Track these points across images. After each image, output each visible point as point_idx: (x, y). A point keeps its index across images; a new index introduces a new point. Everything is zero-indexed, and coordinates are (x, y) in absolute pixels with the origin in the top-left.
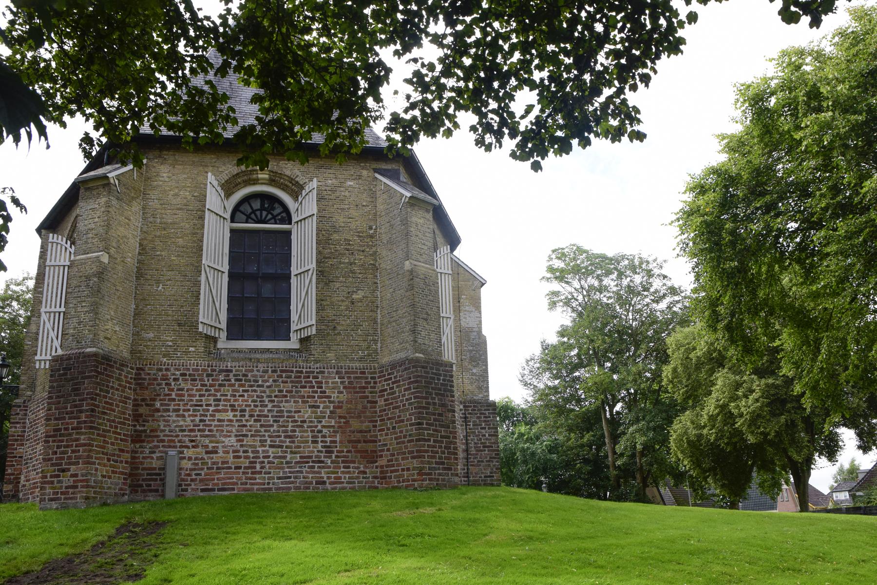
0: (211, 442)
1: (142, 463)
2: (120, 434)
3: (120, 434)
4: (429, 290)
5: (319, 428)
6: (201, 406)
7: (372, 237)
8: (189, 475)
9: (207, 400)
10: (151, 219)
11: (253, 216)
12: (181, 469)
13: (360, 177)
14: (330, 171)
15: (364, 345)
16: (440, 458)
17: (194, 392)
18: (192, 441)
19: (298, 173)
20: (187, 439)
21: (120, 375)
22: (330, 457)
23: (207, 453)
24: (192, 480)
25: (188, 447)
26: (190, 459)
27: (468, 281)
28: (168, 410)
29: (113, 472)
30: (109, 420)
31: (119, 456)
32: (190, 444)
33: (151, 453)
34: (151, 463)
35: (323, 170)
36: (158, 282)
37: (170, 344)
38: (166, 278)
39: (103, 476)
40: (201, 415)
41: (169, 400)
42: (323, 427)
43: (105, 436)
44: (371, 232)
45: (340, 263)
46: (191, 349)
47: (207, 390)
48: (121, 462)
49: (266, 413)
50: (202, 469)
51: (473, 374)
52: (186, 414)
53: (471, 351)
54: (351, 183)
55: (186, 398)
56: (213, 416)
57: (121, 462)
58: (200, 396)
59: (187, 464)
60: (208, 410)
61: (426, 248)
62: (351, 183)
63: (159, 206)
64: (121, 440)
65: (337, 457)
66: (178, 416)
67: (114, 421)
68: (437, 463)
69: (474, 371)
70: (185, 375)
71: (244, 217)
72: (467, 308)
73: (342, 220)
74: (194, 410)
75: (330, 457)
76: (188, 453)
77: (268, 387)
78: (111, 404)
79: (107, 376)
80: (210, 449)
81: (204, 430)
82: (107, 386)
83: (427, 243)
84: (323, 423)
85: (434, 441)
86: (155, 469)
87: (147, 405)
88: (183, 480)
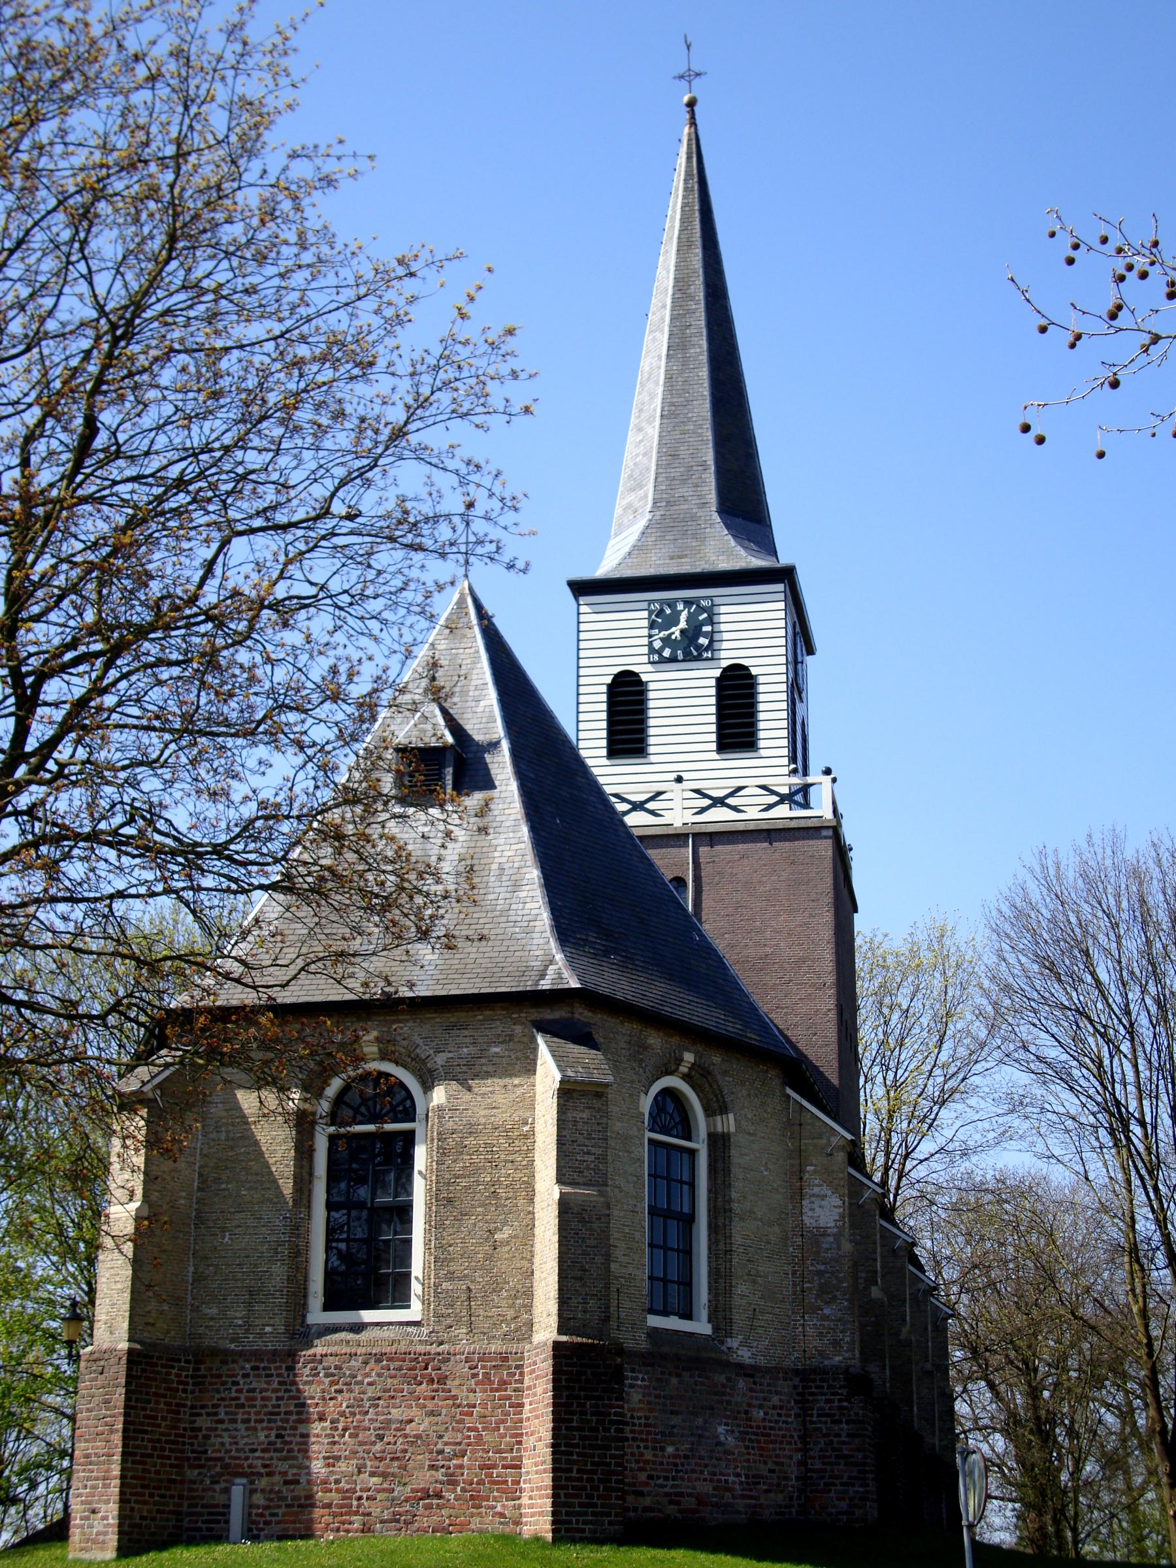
0: (291, 1467)
1: (202, 1498)
2: (169, 1458)
3: (169, 1458)
4: (591, 1229)
5: (440, 1446)
6: (278, 1414)
7: (526, 1137)
8: (262, 1515)
9: (287, 1405)
10: (214, 1135)
11: (363, 1109)
12: (251, 1506)
13: (511, 1038)
14: (466, 1033)
15: (511, 1313)
16: (590, 1497)
17: (269, 1394)
18: (265, 1466)
19: (419, 1041)
20: (259, 1462)
21: (169, 1374)
22: (454, 1491)
23: (286, 1483)
24: (266, 1523)
25: (261, 1475)
26: (263, 1491)
27: (820, 1137)
28: (235, 1421)
29: (158, 1511)
30: (150, 1441)
31: (167, 1489)
32: (263, 1471)
33: (213, 1483)
34: (213, 1498)
35: (455, 1032)
36: (224, 1230)
37: (240, 1322)
38: (235, 1223)
39: (143, 1518)
40: (278, 1428)
41: (237, 1406)
42: (446, 1444)
43: (144, 1463)
44: (526, 1128)
45: (478, 1182)
46: (268, 1329)
47: (286, 1391)
48: (172, 1497)
49: (367, 1423)
50: (279, 1507)
51: (826, 1318)
52: (259, 1426)
53: (820, 1273)
54: (497, 1050)
55: (258, 1403)
56: (295, 1428)
57: (172, 1497)
58: (278, 1399)
59: (259, 1499)
60: (287, 1421)
61: (592, 1158)
62: (497, 1050)
63: (224, 1114)
64: (171, 1466)
65: (464, 1490)
66: (247, 1429)
67: (159, 1441)
68: (581, 1505)
69: (827, 1311)
70: (257, 1368)
71: (350, 1113)
72: (816, 1190)
73: (483, 1113)
74: (269, 1421)
75: (454, 1491)
76: (263, 1483)
77: (370, 1384)
78: (155, 1418)
79: (148, 1378)
80: (290, 1477)
81: (281, 1450)
82: (147, 1394)
83: (593, 1150)
84: (445, 1439)
85: (579, 1471)
86: (217, 1506)
87: (208, 1414)
88: (254, 1522)
